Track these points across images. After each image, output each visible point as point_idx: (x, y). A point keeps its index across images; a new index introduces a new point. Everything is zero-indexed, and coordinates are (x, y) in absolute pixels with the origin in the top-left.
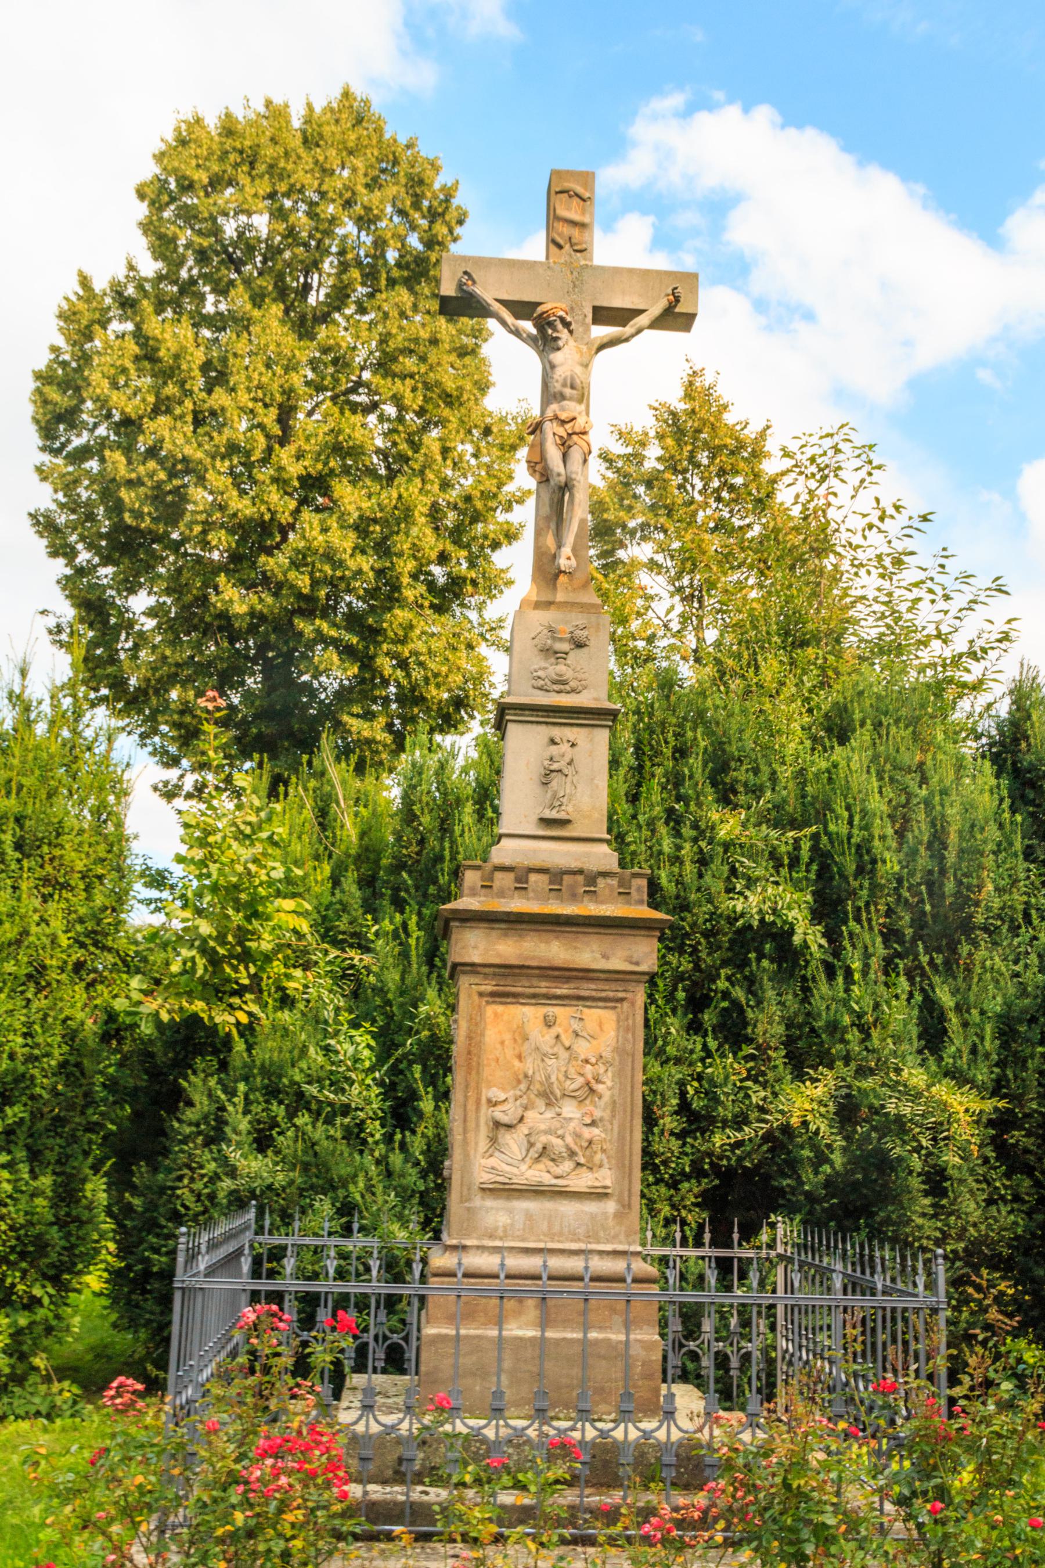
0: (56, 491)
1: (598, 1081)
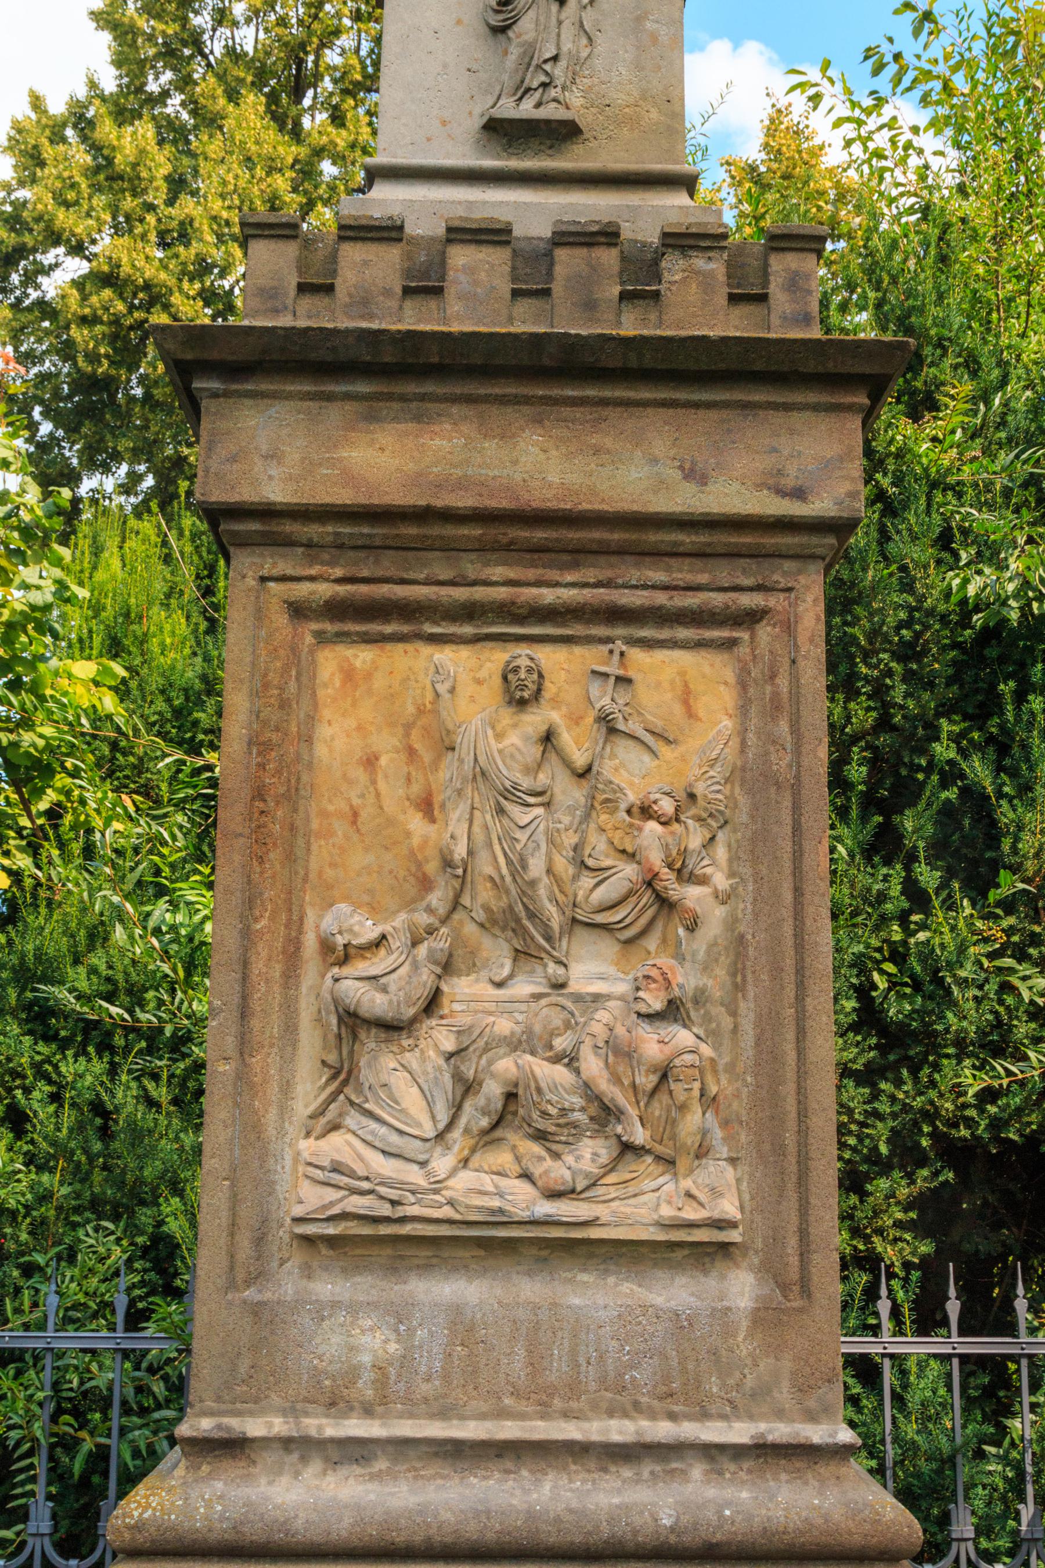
1: (685, 875)
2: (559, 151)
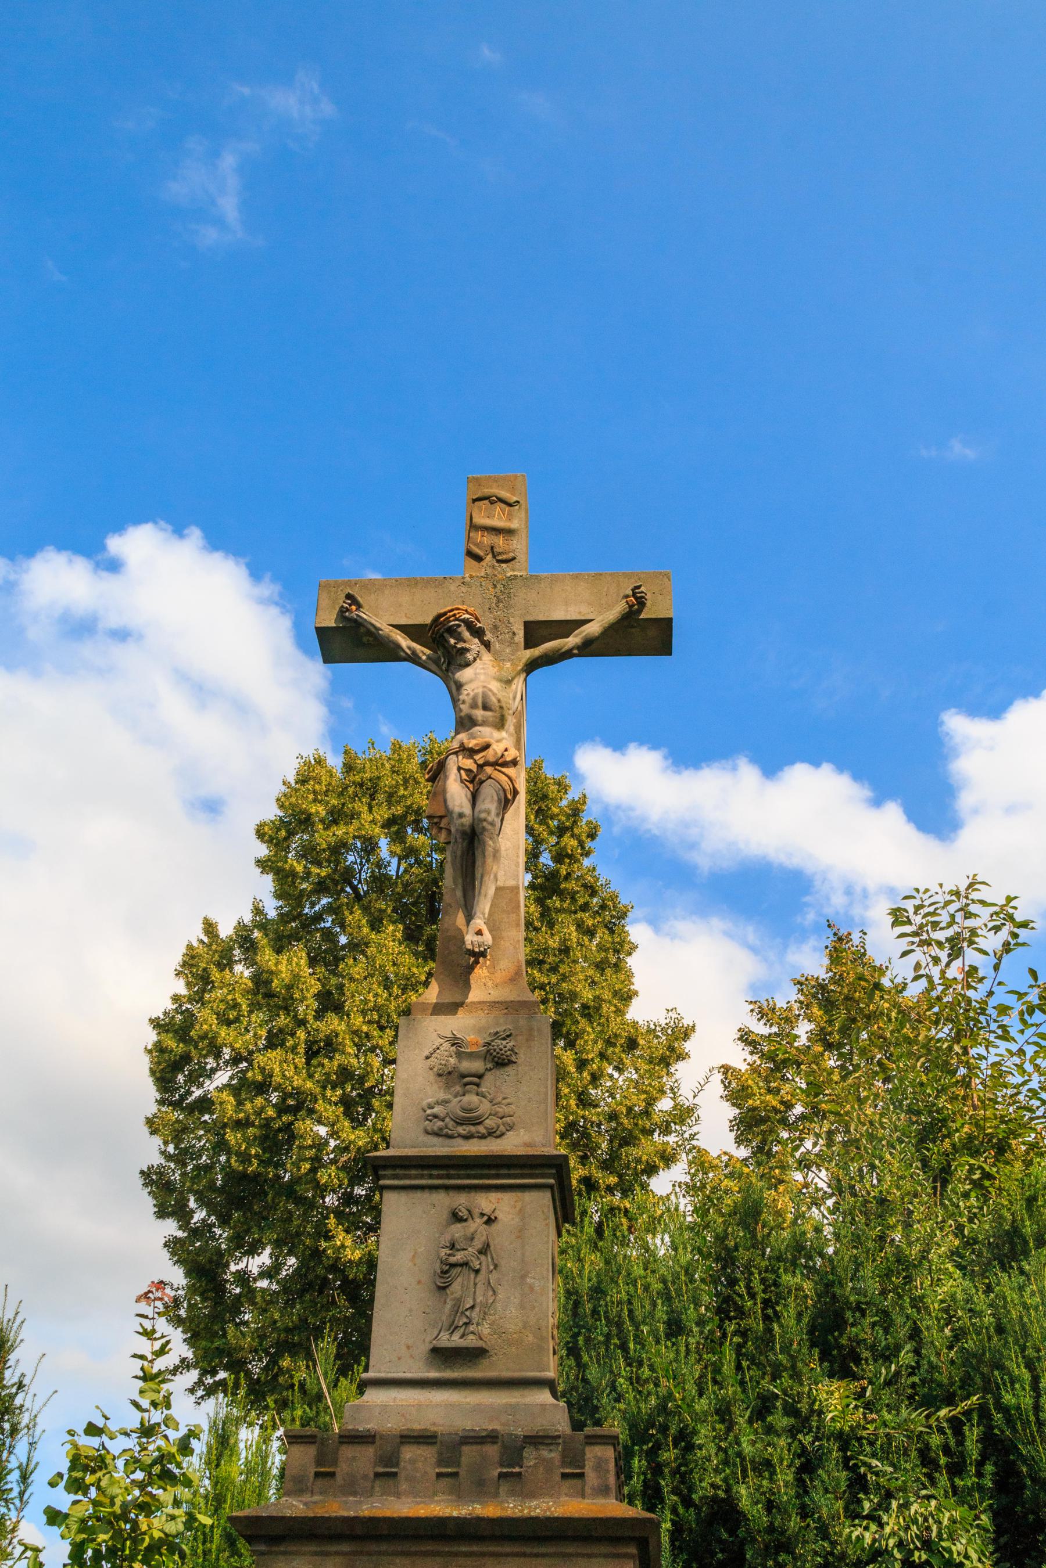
0: (166, 1143)
2: (475, 1364)
